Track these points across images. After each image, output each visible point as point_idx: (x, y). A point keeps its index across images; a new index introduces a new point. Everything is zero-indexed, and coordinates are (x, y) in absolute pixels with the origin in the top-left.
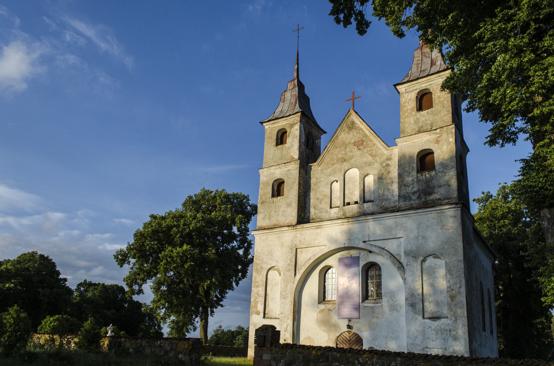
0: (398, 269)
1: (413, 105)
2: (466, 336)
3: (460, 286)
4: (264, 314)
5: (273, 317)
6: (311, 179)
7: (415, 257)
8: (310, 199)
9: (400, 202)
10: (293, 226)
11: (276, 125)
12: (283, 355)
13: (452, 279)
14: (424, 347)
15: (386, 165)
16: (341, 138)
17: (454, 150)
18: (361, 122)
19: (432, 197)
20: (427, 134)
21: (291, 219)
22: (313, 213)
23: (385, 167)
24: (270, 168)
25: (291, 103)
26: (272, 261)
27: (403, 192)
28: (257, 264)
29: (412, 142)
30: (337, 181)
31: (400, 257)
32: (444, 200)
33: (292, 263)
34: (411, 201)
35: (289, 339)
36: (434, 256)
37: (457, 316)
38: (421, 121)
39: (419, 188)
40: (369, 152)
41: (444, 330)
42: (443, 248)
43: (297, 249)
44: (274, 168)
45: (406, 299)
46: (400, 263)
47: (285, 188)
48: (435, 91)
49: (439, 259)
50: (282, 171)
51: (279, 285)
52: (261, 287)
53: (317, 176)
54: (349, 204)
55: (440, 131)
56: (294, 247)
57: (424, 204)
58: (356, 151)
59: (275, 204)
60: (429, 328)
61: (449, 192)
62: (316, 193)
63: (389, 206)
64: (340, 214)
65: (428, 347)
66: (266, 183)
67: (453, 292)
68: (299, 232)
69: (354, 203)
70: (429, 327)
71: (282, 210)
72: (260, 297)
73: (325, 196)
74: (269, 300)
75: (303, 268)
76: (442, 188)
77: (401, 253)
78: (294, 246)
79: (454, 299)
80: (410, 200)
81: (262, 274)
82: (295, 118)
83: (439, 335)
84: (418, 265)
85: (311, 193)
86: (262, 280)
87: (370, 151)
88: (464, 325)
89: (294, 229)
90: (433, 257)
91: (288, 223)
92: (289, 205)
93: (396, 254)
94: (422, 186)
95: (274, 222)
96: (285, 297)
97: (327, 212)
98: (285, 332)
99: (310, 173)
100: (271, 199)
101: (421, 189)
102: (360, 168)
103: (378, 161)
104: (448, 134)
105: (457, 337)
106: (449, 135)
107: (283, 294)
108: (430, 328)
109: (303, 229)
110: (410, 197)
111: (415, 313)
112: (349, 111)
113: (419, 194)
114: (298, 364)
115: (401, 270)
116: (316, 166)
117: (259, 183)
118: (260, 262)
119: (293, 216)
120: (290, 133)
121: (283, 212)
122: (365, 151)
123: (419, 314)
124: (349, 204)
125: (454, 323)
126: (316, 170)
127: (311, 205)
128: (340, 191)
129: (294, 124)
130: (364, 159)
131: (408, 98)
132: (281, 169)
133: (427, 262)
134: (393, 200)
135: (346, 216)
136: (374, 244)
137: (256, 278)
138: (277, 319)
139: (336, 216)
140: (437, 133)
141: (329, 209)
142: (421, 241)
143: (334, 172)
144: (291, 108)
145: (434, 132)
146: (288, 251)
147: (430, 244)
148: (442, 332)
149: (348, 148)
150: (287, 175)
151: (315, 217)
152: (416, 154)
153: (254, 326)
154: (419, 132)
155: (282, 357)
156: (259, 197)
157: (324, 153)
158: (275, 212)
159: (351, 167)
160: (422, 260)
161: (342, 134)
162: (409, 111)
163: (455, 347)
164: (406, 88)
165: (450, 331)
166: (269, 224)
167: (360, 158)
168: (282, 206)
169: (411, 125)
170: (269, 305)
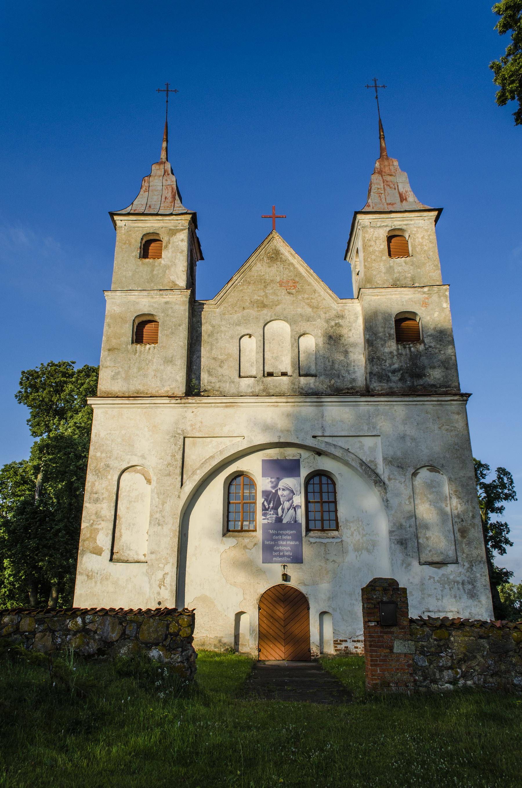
0: (375, 484)
1: (382, 247)
2: (488, 591)
3: (473, 515)
4: (112, 553)
5: (130, 559)
6: (201, 324)
7: (402, 468)
8: (199, 357)
9: (373, 382)
10: (181, 398)
11: (140, 225)
12: (441, 643)
13: (460, 504)
14: (424, 609)
15: (336, 324)
16: (257, 271)
17: (449, 320)
18: (291, 254)
19: (421, 382)
20: (409, 291)
21: (174, 385)
22: (206, 381)
23: (334, 328)
24: (129, 293)
25: (163, 197)
26: (131, 455)
27: (377, 368)
28: (97, 459)
29: (386, 298)
30: (250, 336)
31: (376, 465)
32: (440, 387)
33: (176, 463)
34: (391, 383)
35: (168, 601)
36: (429, 468)
37: (472, 561)
38: (396, 271)
39: (402, 366)
40: (307, 301)
41: (454, 582)
42: (444, 457)
43: (184, 438)
44: (136, 293)
45: (391, 532)
46: (377, 475)
47: (159, 332)
48: (414, 234)
49: (437, 474)
50: (155, 303)
51: (148, 500)
52: (104, 501)
53: (214, 322)
54: (270, 374)
55: (429, 290)
56: (179, 434)
57: (410, 390)
58: (284, 296)
59: (140, 356)
60: (429, 579)
61: (447, 377)
62: (212, 349)
63: (342, 386)
64: (258, 389)
65: (431, 610)
66: (120, 319)
67: (464, 524)
68: (190, 410)
69: (280, 374)
70: (431, 577)
71: (154, 367)
72: (103, 520)
73: (229, 355)
74: (123, 527)
75: (198, 471)
76: (436, 370)
77: (377, 460)
78: (180, 432)
79: (465, 535)
80: (388, 381)
81: (109, 477)
82: (180, 221)
83: (447, 590)
84: (407, 481)
85: (202, 348)
86: (107, 490)
87: (308, 299)
88: (483, 574)
89: (181, 403)
90: (427, 469)
91: (167, 392)
92: (169, 361)
93: (368, 460)
94: (406, 363)
95: (135, 386)
96: (161, 522)
97: (233, 382)
98: (160, 588)
99: (201, 315)
100: (130, 347)
101: (404, 368)
102: (291, 321)
103: (323, 316)
104: (439, 297)
105: (475, 594)
106: (442, 298)
107: (155, 516)
108: (432, 580)
109: (200, 405)
110: (389, 377)
111: (407, 555)
112: (271, 233)
113: (401, 374)
114: (482, 660)
115: (381, 486)
116: (211, 306)
117: (104, 315)
118: (104, 455)
119: (177, 381)
120: (169, 243)
121: (156, 371)
122: (300, 297)
123: (412, 557)
124: (270, 374)
125: (468, 571)
126: (211, 311)
127: (202, 368)
128: (257, 353)
129: (177, 230)
130: (299, 310)
131: (375, 235)
132: (153, 298)
133: (418, 476)
134: (349, 379)
135: (269, 393)
136: (331, 442)
137: (93, 484)
138: (139, 562)
139: (250, 390)
140: (424, 293)
141: (237, 379)
142: (409, 444)
143: (246, 321)
144: (166, 204)
145: (420, 289)
146: (167, 441)
147: (423, 449)
148: (451, 586)
149: (269, 288)
150: (164, 311)
151: (209, 388)
152: (394, 316)
153: (88, 576)
154: (395, 285)
155: (439, 646)
156: (104, 338)
157: (228, 288)
158: (140, 369)
159: (276, 318)
160: (412, 472)
161: (259, 265)
162: (377, 253)
163: (473, 609)
164: (371, 221)
165: (463, 584)
166: (124, 389)
167: (292, 307)
168: (155, 360)
169: (383, 275)
170: (121, 536)
